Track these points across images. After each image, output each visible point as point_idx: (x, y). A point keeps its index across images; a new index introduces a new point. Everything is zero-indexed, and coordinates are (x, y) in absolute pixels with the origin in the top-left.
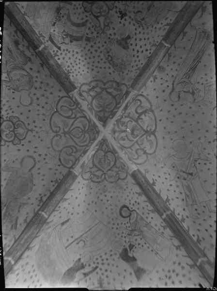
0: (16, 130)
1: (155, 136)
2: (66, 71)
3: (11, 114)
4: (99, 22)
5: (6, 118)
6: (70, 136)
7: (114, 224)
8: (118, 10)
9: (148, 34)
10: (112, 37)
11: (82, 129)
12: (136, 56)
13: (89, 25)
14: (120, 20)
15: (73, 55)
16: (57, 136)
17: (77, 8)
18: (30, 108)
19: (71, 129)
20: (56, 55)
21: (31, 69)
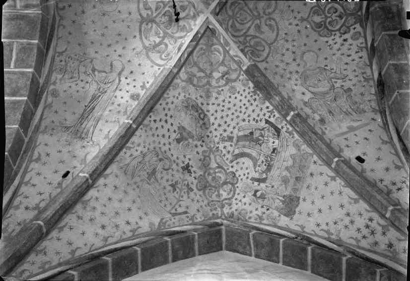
0: (324, 19)
1: (140, 15)
2: (258, 92)
3: (330, 40)
5: (335, 35)
6: (252, 12)
7: (160, 196)
8: (193, 175)
9: (154, 142)
11: (236, 20)
12: (169, 116)
14: (190, 162)
15: (249, 116)
16: (269, 14)
17: (244, 175)
19: (250, 23)
21: (303, 94)
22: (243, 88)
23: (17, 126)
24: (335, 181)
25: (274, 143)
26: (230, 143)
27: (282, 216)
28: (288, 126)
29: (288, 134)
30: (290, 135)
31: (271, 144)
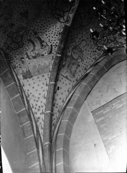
4: (23, 34)
10: (26, 22)
13: (29, 38)
15: (49, 36)
18: (85, 39)
20: (56, 46)
22: (59, 27)
23: (64, 134)
24: (47, 86)
25: (45, 53)
26: (34, 34)
27: (22, 75)
28: (55, 56)
29: (52, 57)
30: (52, 58)
31: (44, 52)
